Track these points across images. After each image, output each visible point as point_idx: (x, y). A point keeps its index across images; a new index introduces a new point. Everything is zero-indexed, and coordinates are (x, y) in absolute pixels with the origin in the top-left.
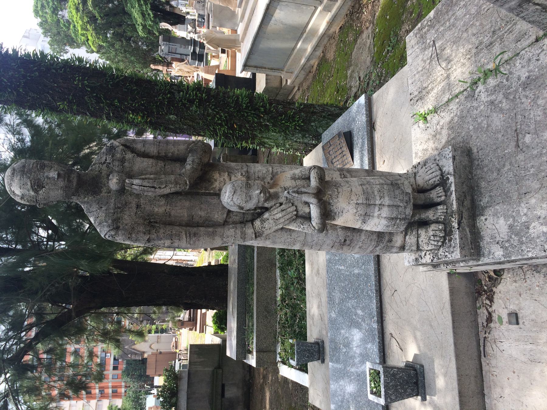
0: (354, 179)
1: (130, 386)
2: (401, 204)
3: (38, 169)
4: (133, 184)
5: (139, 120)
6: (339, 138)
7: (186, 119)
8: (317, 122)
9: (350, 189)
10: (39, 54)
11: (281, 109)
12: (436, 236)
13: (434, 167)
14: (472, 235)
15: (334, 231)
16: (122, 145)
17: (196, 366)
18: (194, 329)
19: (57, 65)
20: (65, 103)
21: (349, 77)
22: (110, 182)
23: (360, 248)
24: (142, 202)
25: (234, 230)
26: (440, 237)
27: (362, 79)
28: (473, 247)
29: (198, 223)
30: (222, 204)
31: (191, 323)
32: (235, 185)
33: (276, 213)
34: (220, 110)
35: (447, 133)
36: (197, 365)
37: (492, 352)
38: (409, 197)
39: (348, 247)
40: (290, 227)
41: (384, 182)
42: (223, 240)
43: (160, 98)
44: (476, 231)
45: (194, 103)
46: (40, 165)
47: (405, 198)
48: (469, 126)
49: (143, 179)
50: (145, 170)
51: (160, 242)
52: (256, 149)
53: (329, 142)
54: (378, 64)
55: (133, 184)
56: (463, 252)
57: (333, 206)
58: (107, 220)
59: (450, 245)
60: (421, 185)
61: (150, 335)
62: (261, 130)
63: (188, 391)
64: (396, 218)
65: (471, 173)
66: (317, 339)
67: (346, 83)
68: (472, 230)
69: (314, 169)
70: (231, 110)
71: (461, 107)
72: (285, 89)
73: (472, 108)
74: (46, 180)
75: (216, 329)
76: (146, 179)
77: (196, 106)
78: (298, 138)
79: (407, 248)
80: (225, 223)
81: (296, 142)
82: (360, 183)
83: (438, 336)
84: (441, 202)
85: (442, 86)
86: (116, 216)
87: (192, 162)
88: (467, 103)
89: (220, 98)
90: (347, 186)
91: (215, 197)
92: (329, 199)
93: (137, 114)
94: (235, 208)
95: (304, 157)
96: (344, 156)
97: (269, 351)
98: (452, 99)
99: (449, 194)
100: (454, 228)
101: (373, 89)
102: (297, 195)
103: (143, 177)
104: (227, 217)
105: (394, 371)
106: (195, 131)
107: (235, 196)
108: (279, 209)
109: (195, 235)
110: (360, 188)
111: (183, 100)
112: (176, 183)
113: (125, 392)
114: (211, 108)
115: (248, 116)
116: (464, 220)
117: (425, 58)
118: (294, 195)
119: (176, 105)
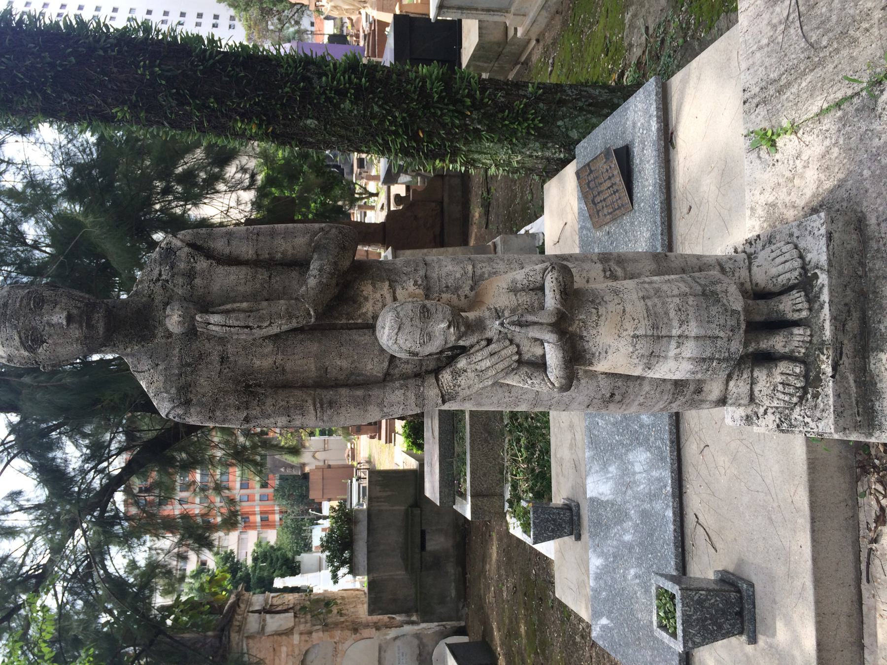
0: (630, 284)
1: (286, 512)
2: (722, 334)
3: (30, 309)
4: (209, 324)
5: (254, 131)
6: (607, 159)
7: (335, 125)
10: (74, 22)
11: (503, 99)
12: (788, 385)
14: (860, 387)
15: (591, 379)
16: (189, 245)
17: (379, 504)
18: (377, 436)
19: (105, 41)
20: (126, 109)
21: (627, 26)
22: (167, 320)
23: (640, 405)
24: (230, 351)
25: (402, 391)
26: (797, 388)
27: (651, 31)
28: (861, 410)
29: (336, 379)
32: (401, 315)
33: (481, 360)
34: (394, 106)
35: (816, 177)
36: (381, 502)
37: (883, 577)
38: (738, 320)
39: (619, 405)
41: (688, 290)
43: (287, 89)
44: (868, 379)
45: (347, 96)
46: (34, 300)
47: (729, 323)
48: (863, 170)
49: (227, 312)
50: (233, 290)
51: (267, 421)
52: (460, 170)
53: (588, 164)
54: (682, 6)
55: (209, 324)
56: (841, 422)
57: (588, 341)
58: (168, 388)
59: (816, 405)
60: (762, 284)
61: (312, 438)
62: (466, 139)
63: (368, 541)
64: (710, 359)
65: (862, 264)
66: (568, 499)
67: (623, 37)
68: (860, 378)
70: (412, 105)
71: (847, 128)
72: (514, 45)
73: (870, 134)
74: (47, 328)
76: (233, 311)
77: (351, 102)
80: (387, 378)
81: (530, 156)
82: (641, 294)
83: (782, 540)
84: (801, 319)
85: (808, 80)
86: (183, 380)
87: (320, 271)
88: (859, 121)
89: (392, 84)
90: (616, 301)
91: (366, 331)
92: (580, 328)
93: (250, 120)
94: (403, 354)
96: (615, 193)
97: (493, 495)
98: (828, 110)
99: (816, 306)
100: (824, 373)
101: (672, 52)
102: (518, 329)
103: (228, 307)
104: (389, 366)
105: (701, 595)
106: (352, 146)
107: (400, 335)
108: (486, 352)
109: (331, 404)
110: (640, 305)
111: (328, 92)
112: (290, 316)
113: (281, 519)
114: (376, 103)
115: (442, 114)
116: (844, 358)
117: (775, 21)
118: (513, 328)
119: (315, 101)
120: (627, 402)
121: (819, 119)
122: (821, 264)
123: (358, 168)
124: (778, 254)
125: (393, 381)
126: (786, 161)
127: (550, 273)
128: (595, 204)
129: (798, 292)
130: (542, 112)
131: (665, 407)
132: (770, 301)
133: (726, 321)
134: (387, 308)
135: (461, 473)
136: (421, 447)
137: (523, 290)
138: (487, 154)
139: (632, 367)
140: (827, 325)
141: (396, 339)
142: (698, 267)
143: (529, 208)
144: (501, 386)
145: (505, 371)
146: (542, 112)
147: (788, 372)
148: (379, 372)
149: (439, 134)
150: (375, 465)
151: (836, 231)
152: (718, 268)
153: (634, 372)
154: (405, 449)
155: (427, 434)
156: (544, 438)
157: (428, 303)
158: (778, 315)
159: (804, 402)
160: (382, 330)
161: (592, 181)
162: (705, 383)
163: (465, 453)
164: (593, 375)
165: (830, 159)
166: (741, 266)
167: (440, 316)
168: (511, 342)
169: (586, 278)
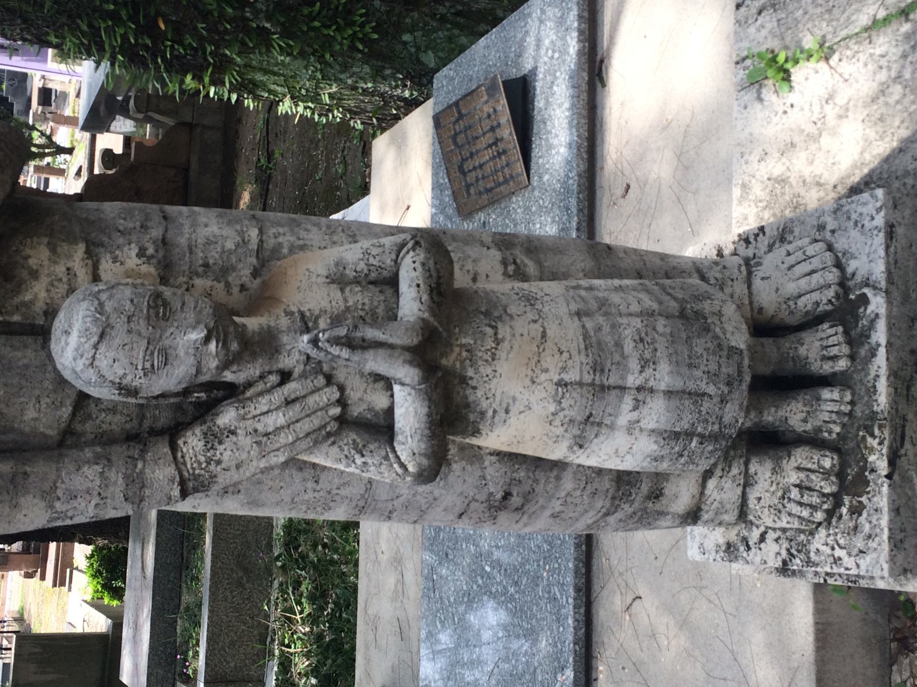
0: (553, 288)
2: (711, 389)
8: (420, 33)
9: (537, 327)
12: (810, 489)
13: (820, 256)
15: (472, 464)
18: (38, 574)
23: (554, 516)
25: (99, 468)
26: (824, 495)
30: (55, 368)
31: (31, 557)
32: (109, 307)
38: (740, 366)
39: (516, 516)
40: (318, 459)
41: (655, 306)
42: (51, 507)
47: (724, 370)
52: (229, 99)
53: (456, 104)
56: (900, 558)
57: (475, 388)
62: (244, 44)
69: (413, 249)
75: (97, 591)
78: (361, 78)
79: (705, 517)
81: (354, 88)
82: (574, 307)
90: (530, 316)
91: (29, 340)
94: (106, 390)
95: (374, 136)
96: (499, 154)
98: (886, 20)
99: (863, 352)
102: (345, 353)
104: (74, 414)
107: (102, 348)
108: (277, 397)
110: (573, 327)
116: (908, 445)
118: (335, 350)
120: (531, 511)
121: (870, 37)
122: (874, 278)
123: (39, 104)
124: (800, 259)
125: (79, 446)
126: (807, 107)
127: (411, 253)
128: (464, 173)
129: (831, 327)
130: (378, 14)
131: (595, 522)
132: (781, 341)
133: (720, 366)
134: (78, 294)
135: (189, 642)
136: (118, 593)
137: (356, 281)
138: (279, 75)
139: (550, 443)
140: (882, 386)
141: (94, 358)
142: (663, 272)
143: (338, 188)
144: (301, 469)
145: (313, 437)
146: (378, 14)
147: (809, 466)
148: (50, 427)
149: (196, 28)
150: (29, 625)
151: (900, 224)
152: (696, 275)
153: (553, 451)
154: (89, 598)
155: (132, 571)
156: (344, 582)
157: (167, 292)
158: (795, 365)
159: (834, 520)
160: (63, 339)
161: (460, 132)
162: (667, 480)
163: (200, 606)
164: (474, 455)
165: (887, 104)
166: (734, 277)
167: (190, 316)
168: (330, 380)
169: (472, 272)
